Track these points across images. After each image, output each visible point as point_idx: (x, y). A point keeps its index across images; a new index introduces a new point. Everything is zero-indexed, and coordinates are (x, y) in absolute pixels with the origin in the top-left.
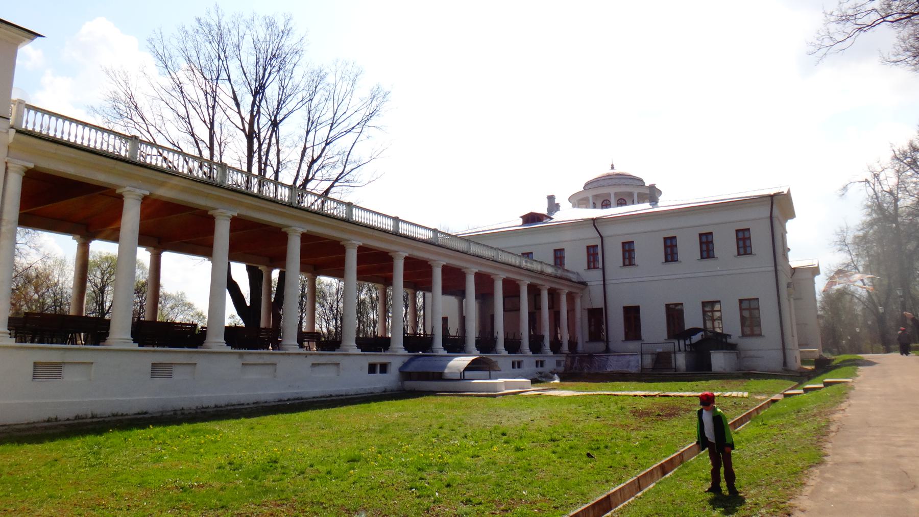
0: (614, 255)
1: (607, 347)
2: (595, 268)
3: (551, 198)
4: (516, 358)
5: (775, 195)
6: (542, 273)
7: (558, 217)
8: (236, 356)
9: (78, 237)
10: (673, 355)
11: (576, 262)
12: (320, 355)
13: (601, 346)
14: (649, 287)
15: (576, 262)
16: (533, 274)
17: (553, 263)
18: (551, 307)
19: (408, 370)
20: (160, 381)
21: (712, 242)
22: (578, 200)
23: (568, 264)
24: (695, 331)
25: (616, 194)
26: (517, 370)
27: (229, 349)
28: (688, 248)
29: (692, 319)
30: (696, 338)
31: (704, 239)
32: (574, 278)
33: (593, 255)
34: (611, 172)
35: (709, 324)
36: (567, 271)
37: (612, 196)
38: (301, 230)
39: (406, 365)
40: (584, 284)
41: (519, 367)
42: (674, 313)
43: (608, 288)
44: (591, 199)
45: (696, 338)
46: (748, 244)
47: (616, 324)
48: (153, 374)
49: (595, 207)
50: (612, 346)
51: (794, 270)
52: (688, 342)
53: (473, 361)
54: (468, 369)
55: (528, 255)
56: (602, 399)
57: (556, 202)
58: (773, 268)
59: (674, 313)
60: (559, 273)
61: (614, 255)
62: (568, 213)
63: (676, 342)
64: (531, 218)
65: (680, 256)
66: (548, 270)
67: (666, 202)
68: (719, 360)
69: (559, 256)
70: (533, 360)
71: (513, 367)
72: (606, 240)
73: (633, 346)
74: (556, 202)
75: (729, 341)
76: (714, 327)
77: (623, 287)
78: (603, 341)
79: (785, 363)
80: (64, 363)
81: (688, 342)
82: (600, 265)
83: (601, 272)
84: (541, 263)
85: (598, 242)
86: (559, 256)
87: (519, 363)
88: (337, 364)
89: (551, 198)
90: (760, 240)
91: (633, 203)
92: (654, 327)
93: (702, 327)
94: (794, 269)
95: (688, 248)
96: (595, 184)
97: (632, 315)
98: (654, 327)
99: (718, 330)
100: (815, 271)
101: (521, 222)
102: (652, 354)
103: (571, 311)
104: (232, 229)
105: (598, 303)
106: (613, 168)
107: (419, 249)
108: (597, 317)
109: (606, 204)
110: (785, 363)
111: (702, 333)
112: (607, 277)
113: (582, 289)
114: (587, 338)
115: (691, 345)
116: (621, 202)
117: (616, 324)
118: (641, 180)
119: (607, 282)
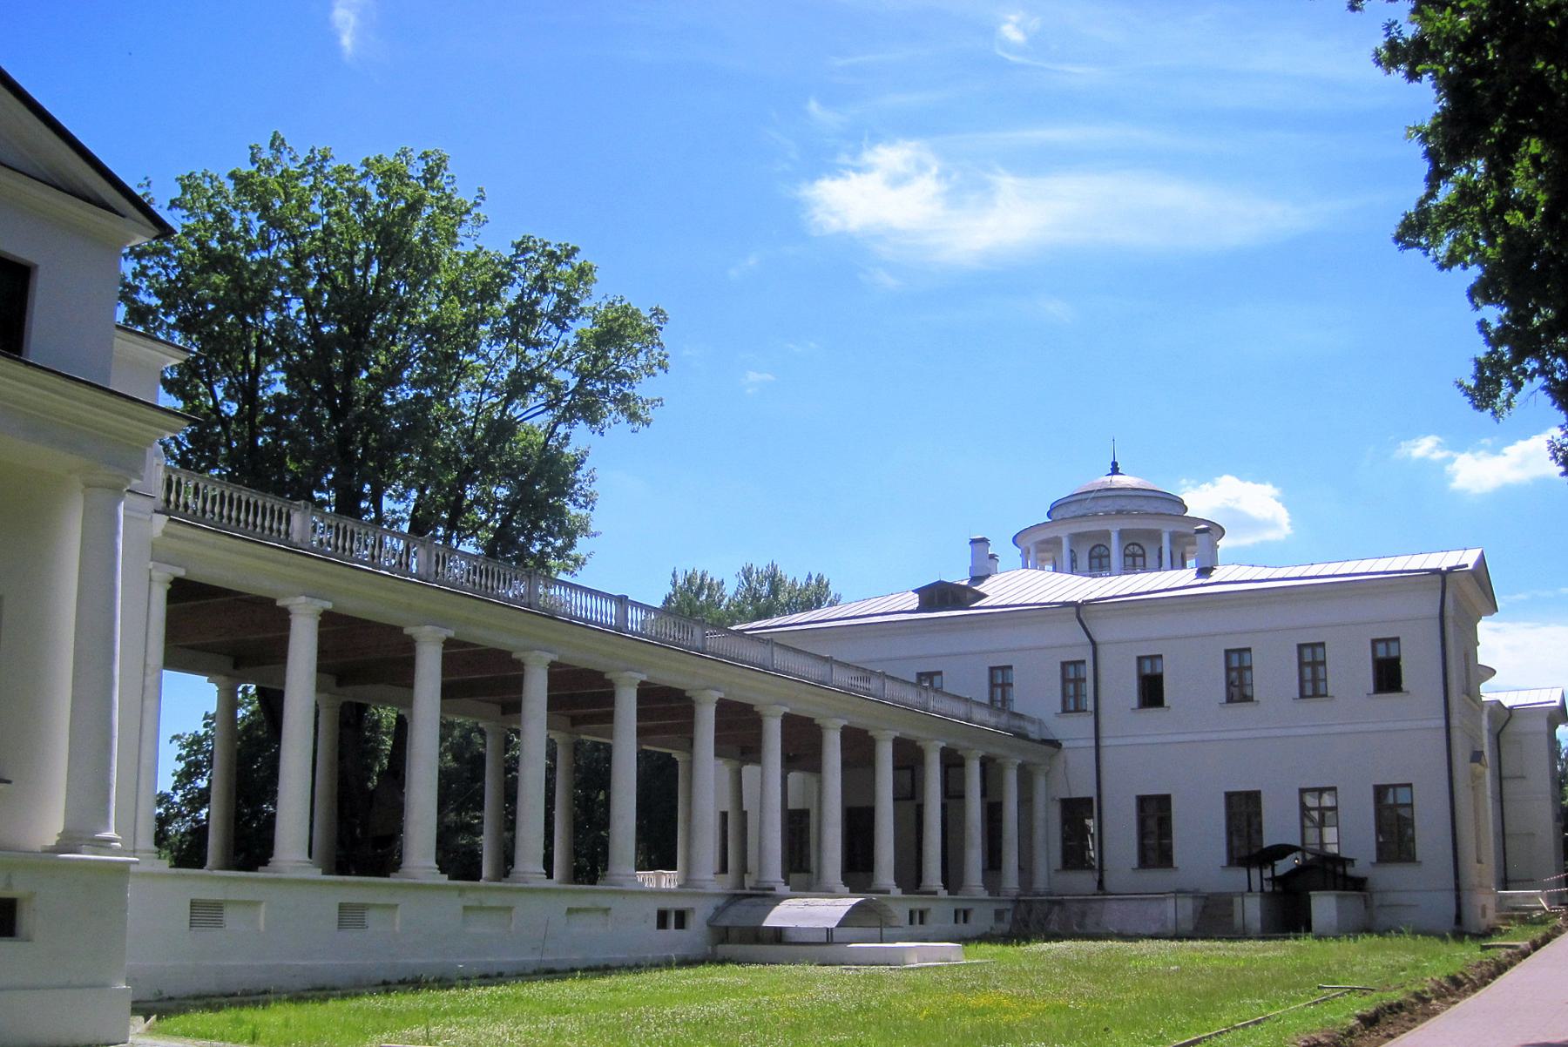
1: (1101, 883)
2: (1077, 710)
4: (917, 903)
5: (1450, 570)
8: (456, 894)
9: (223, 678)
10: (1238, 900)
11: (1037, 697)
12: (573, 891)
13: (1083, 881)
14: (1190, 756)
17: (986, 700)
19: (725, 922)
20: (353, 935)
22: (1039, 547)
24: (1283, 851)
25: (1122, 534)
26: (918, 929)
28: (1274, 673)
29: (1278, 826)
30: (1283, 866)
33: (1076, 686)
34: (1105, 480)
35: (1312, 835)
36: (1020, 716)
38: (549, 657)
40: (1056, 744)
42: (1243, 809)
43: (1104, 753)
45: (1283, 866)
47: (1120, 835)
49: (1073, 569)
50: (1111, 882)
51: (1504, 717)
52: (1267, 873)
53: (854, 906)
54: (843, 923)
55: (927, 679)
56: (1104, 972)
58: (1442, 723)
59: (1243, 809)
61: (1121, 687)
62: (1018, 585)
63: (1244, 872)
64: (937, 596)
65: (1258, 692)
67: (1230, 574)
68: (1324, 906)
69: (1000, 679)
70: (950, 909)
71: (911, 922)
72: (1102, 651)
73: (1156, 878)
75: (1350, 871)
76: (1322, 844)
77: (1136, 755)
78: (1091, 868)
79: (1459, 918)
80: (227, 902)
81: (1267, 873)
82: (1090, 705)
84: (966, 700)
86: (1000, 679)
87: (922, 913)
88: (606, 911)
90: (1418, 667)
91: (1160, 568)
92: (1200, 839)
93: (1297, 842)
94: (1511, 708)
96: (1074, 510)
97: (1155, 814)
98: (1200, 839)
99: (1333, 849)
101: (913, 601)
102: (1195, 898)
103: (1026, 801)
105: (1083, 788)
106: (1115, 470)
109: (1098, 564)
110: (1459, 918)
111: (1299, 855)
115: (1274, 879)
116: (1135, 561)
117: (1120, 835)
119: (1104, 742)
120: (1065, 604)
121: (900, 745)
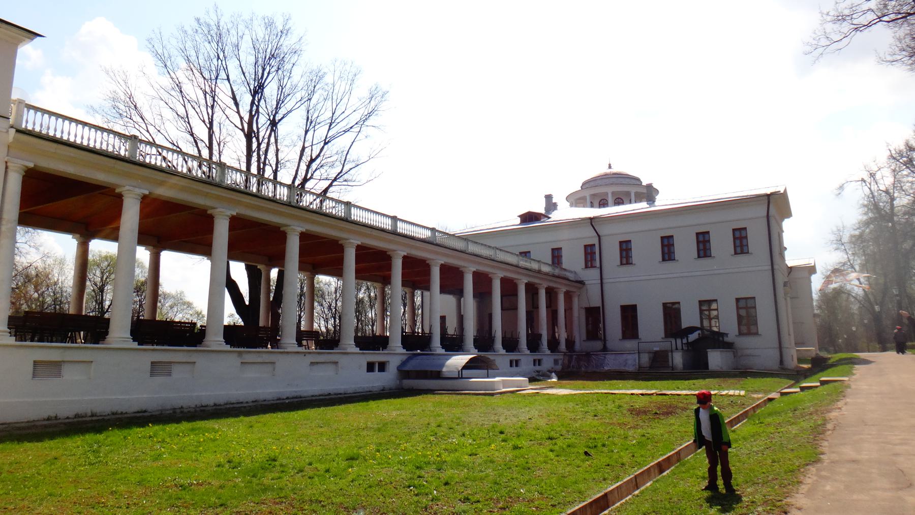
0: (611, 254)
1: (605, 345)
2: (592, 267)
3: (549, 198)
4: (514, 356)
5: (772, 194)
6: (539, 272)
7: (556, 217)
8: (235, 355)
9: (78, 236)
10: (670, 354)
11: (573, 261)
12: (319, 353)
13: (598, 345)
14: (646, 286)
15: (573, 261)
16: (531, 273)
17: (550, 262)
18: (548, 306)
19: (406, 368)
20: (159, 380)
21: (709, 241)
22: (576, 200)
23: (566, 263)
24: (692, 330)
25: (613, 193)
26: (514, 369)
27: (228, 348)
28: (685, 247)
29: (689, 317)
30: (693, 337)
31: (701, 238)
32: (571, 277)
33: (591, 254)
34: (609, 171)
35: (706, 323)
36: (565, 270)
37: (610, 195)
38: (300, 229)
39: (404, 363)
40: (582, 283)
41: (517, 366)
42: (671, 312)
43: (606, 287)
44: (588, 198)
45: (693, 337)
46: (744, 243)
47: (613, 323)
48: (153, 373)
49: (592, 206)
50: (609, 345)
51: (791, 269)
52: (685, 341)
53: (471, 359)
54: (465, 367)
55: (525, 254)
57: (554, 201)
58: (770, 267)
59: (671, 312)
60: (557, 272)
61: (611, 254)
62: (565, 213)
63: (673, 341)
64: (529, 218)
65: (677, 255)
66: (546, 269)
67: (663, 202)
68: (716, 359)
69: (556, 255)
70: (531, 359)
71: (511, 366)
72: (603, 240)
73: (630, 344)
74: (554, 201)
75: (726, 339)
76: (711, 326)
77: (620, 286)
78: (600, 339)
79: (781, 362)
80: (64, 362)
81: (685, 341)
82: (598, 264)
83: (599, 271)
84: (539, 262)
85: (595, 241)
86: (556, 255)
87: (517, 361)
88: (336, 363)
89: (549, 198)
90: (756, 239)
91: (630, 203)
92: (651, 325)
93: (699, 326)
94: (791, 268)
95: (685, 247)
96: (592, 183)
97: (629, 313)
98: (651, 325)
99: (715, 329)
100: (812, 270)
101: (518, 221)
102: (649, 353)
103: (569, 309)
104: (231, 228)
105: (596, 302)
106: (610, 167)
107: (417, 248)
108: (594, 315)
109: (603, 204)
110: (781, 362)
111: (699, 332)
112: (604, 276)
113: (580, 288)
114: (584, 337)
115: (688, 343)
116: (619, 202)
117: (613, 323)
118: (638, 180)
119: (604, 281)
120: (583, 219)
121: (477, 275)
